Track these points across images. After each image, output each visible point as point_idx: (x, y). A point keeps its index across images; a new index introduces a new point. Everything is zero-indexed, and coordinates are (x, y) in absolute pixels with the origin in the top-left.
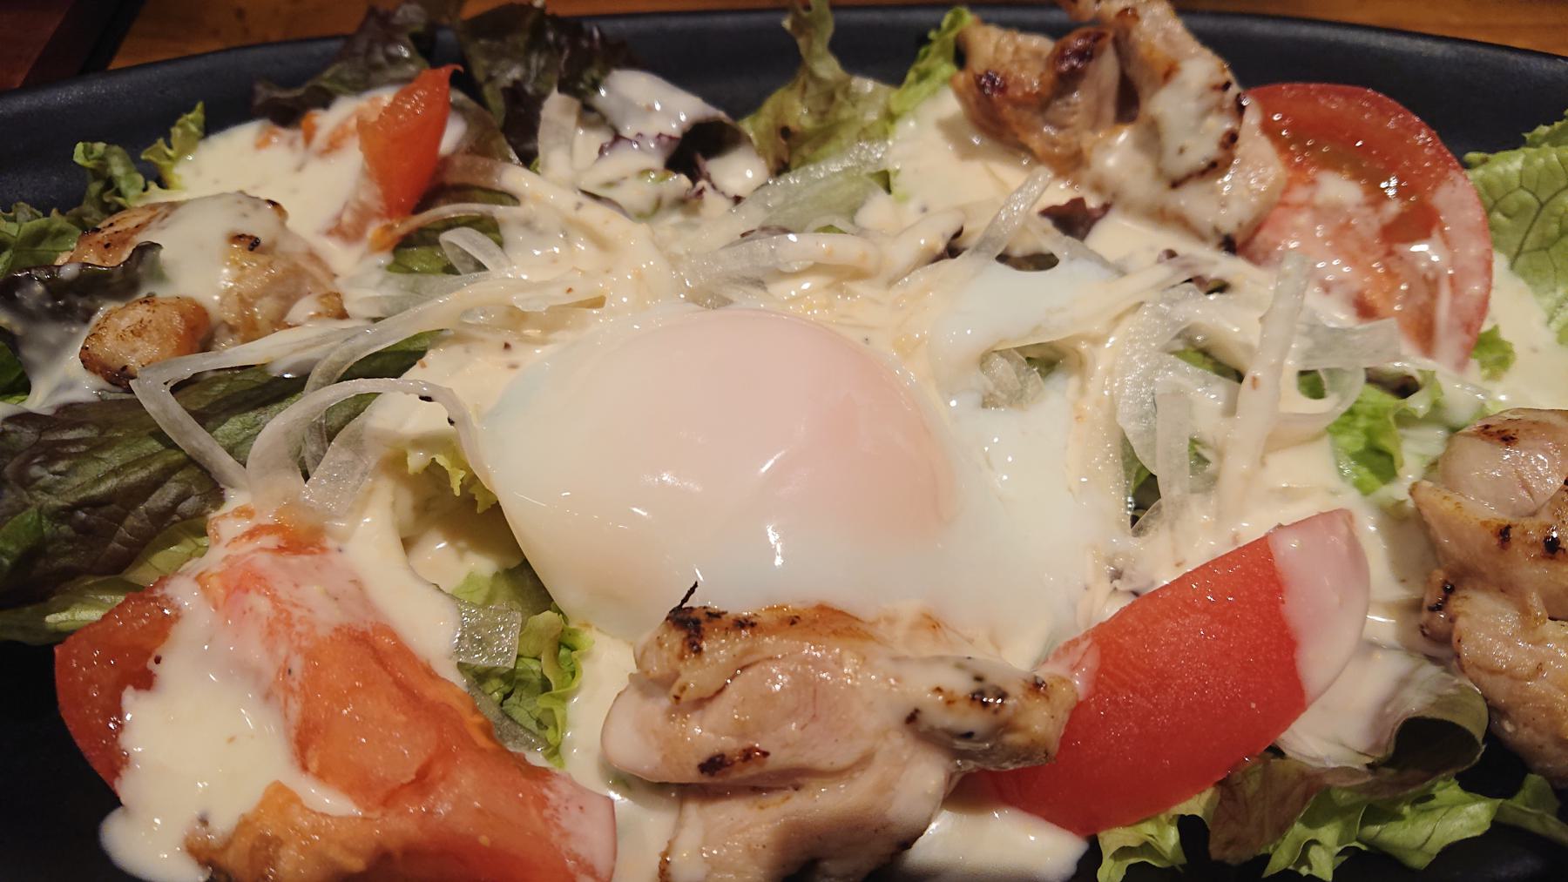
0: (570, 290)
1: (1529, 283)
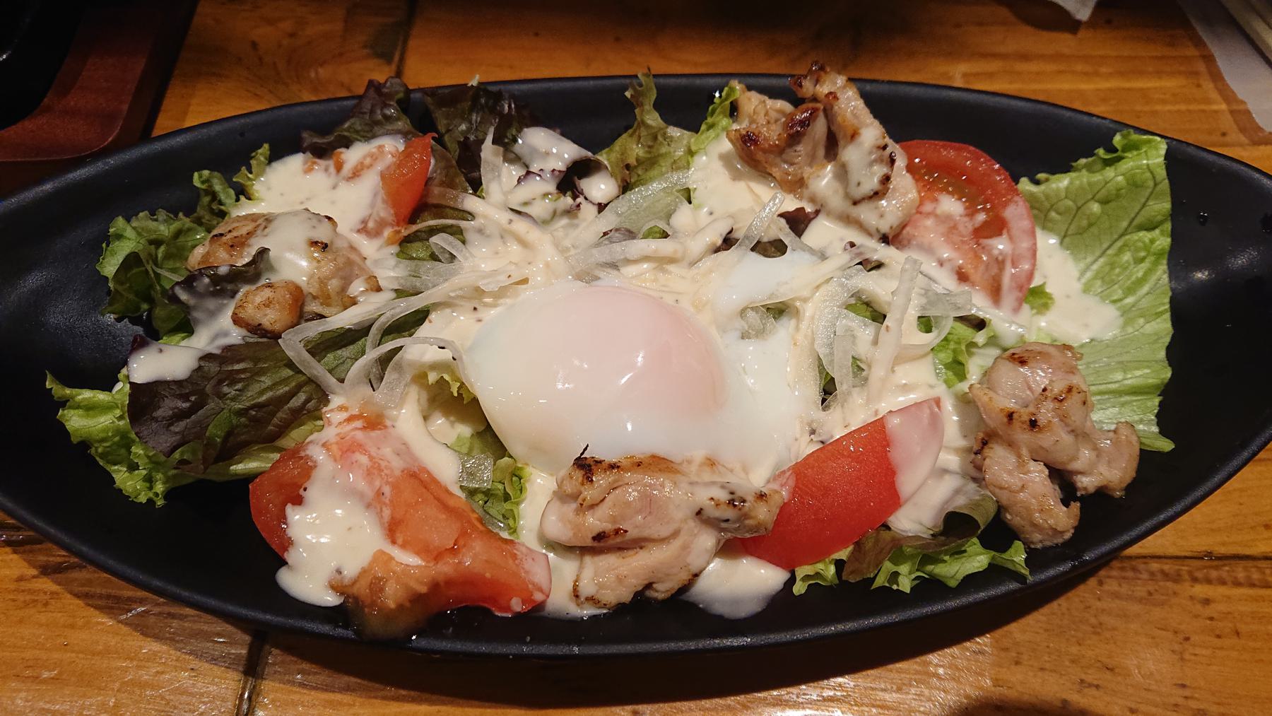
0: (510, 276)
1: (1072, 253)
